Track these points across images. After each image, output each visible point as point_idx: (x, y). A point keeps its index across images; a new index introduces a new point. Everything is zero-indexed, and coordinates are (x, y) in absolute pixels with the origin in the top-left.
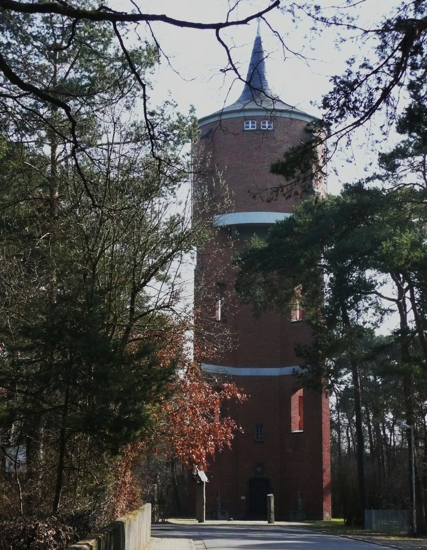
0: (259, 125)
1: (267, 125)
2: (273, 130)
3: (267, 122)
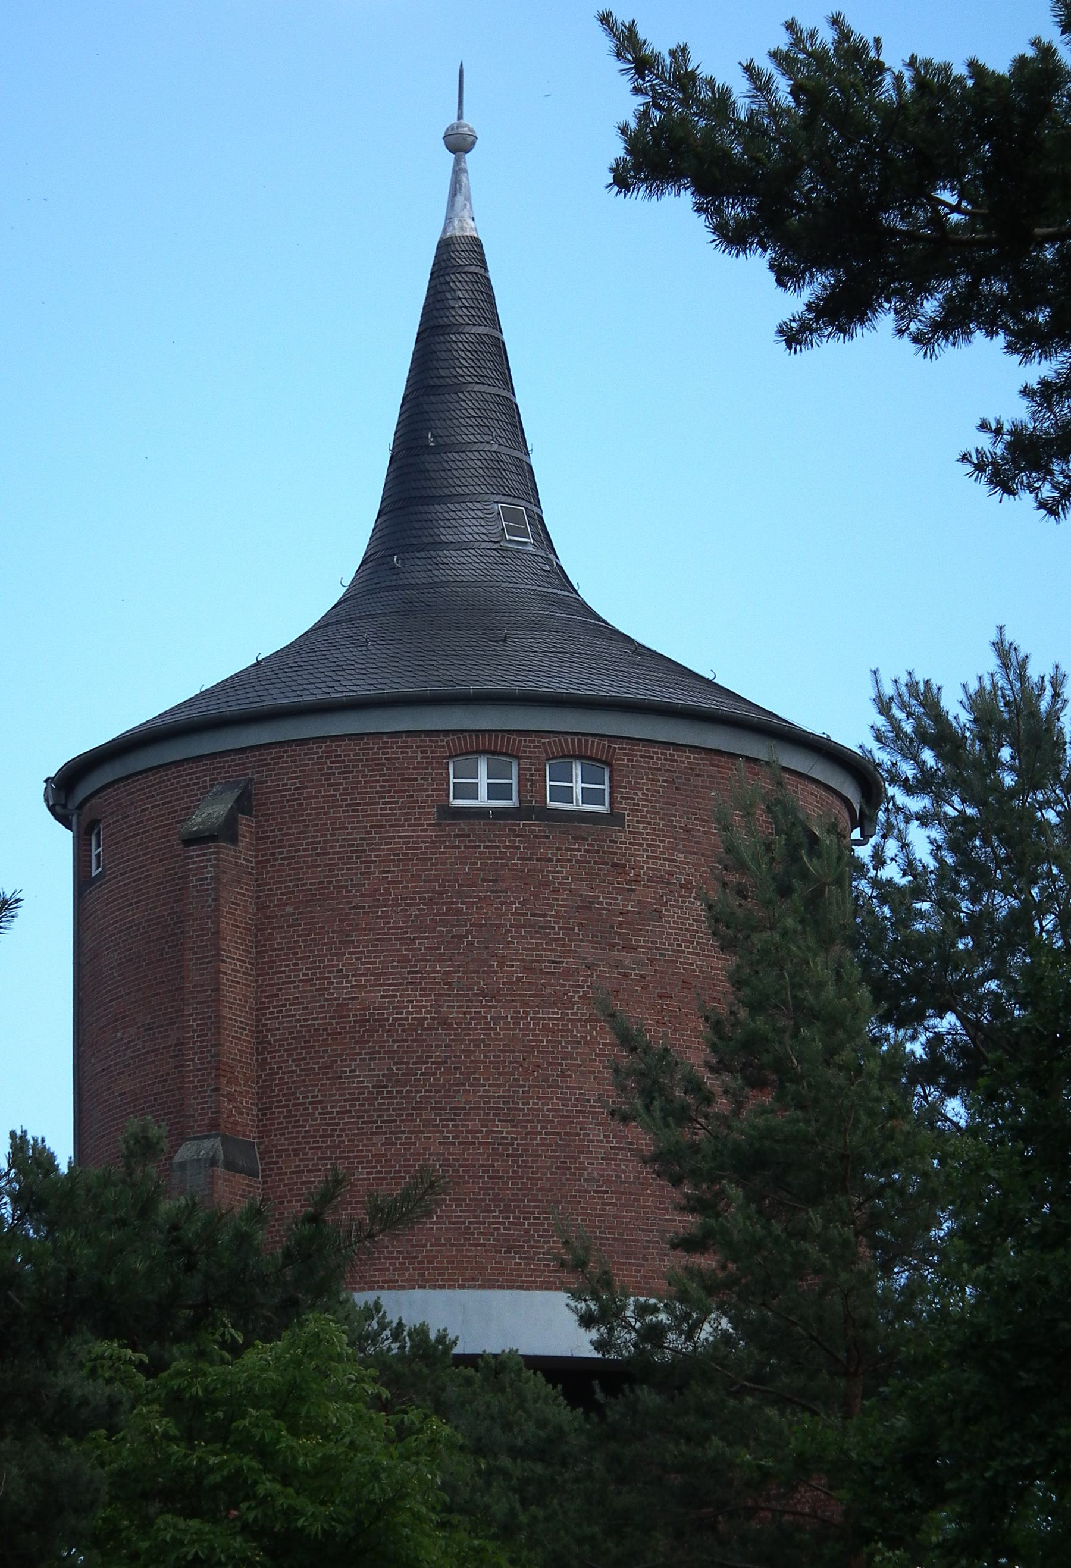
0: (531, 783)
1: (578, 786)
2: (613, 818)
3: (577, 770)
